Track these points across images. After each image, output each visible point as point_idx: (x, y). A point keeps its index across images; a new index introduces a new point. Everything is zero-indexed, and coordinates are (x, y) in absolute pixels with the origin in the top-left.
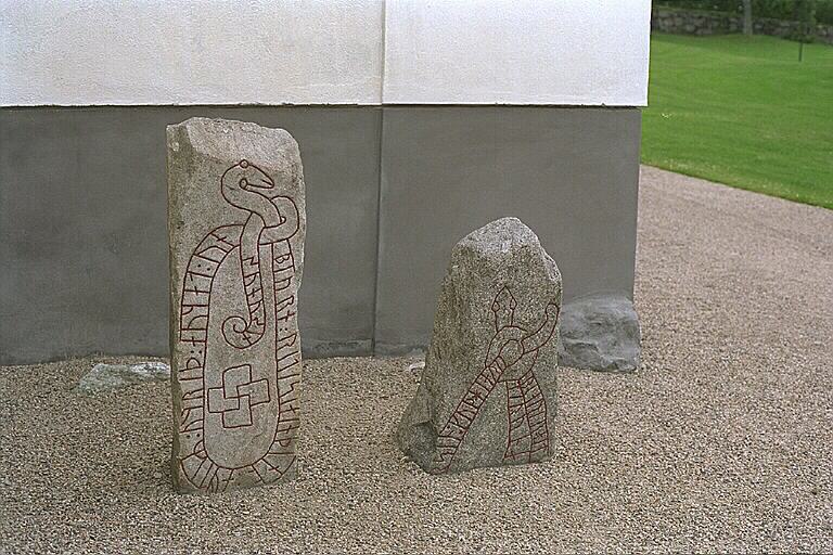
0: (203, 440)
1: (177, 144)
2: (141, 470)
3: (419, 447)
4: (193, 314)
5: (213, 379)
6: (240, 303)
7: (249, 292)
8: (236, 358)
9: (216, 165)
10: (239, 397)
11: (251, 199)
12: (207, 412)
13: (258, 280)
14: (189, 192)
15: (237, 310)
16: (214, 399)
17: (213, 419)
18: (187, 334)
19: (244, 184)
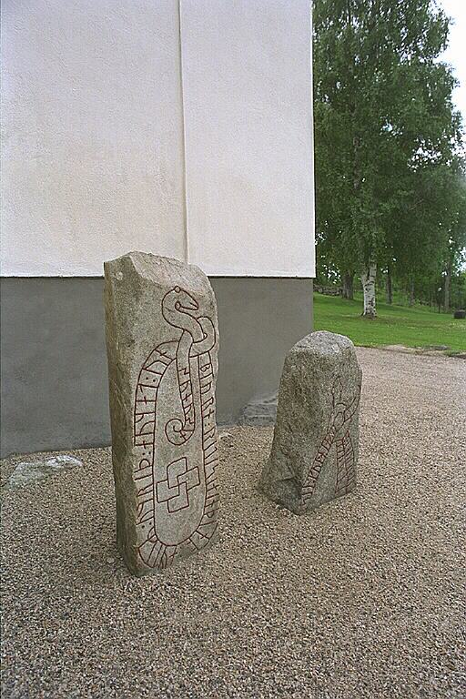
0: (154, 527)
1: (121, 274)
2: (92, 556)
3: (286, 496)
4: (144, 421)
5: (160, 474)
6: (177, 408)
7: (184, 397)
8: (175, 455)
9: (158, 290)
10: (179, 485)
11: (183, 320)
12: (156, 502)
13: (189, 386)
14: (138, 313)
15: (176, 414)
16: (163, 492)
17: (162, 507)
18: (139, 439)
19: (179, 306)
